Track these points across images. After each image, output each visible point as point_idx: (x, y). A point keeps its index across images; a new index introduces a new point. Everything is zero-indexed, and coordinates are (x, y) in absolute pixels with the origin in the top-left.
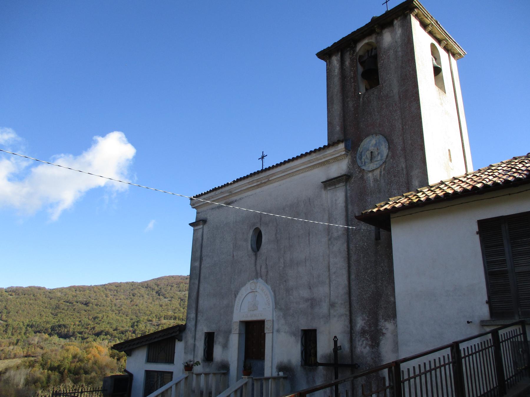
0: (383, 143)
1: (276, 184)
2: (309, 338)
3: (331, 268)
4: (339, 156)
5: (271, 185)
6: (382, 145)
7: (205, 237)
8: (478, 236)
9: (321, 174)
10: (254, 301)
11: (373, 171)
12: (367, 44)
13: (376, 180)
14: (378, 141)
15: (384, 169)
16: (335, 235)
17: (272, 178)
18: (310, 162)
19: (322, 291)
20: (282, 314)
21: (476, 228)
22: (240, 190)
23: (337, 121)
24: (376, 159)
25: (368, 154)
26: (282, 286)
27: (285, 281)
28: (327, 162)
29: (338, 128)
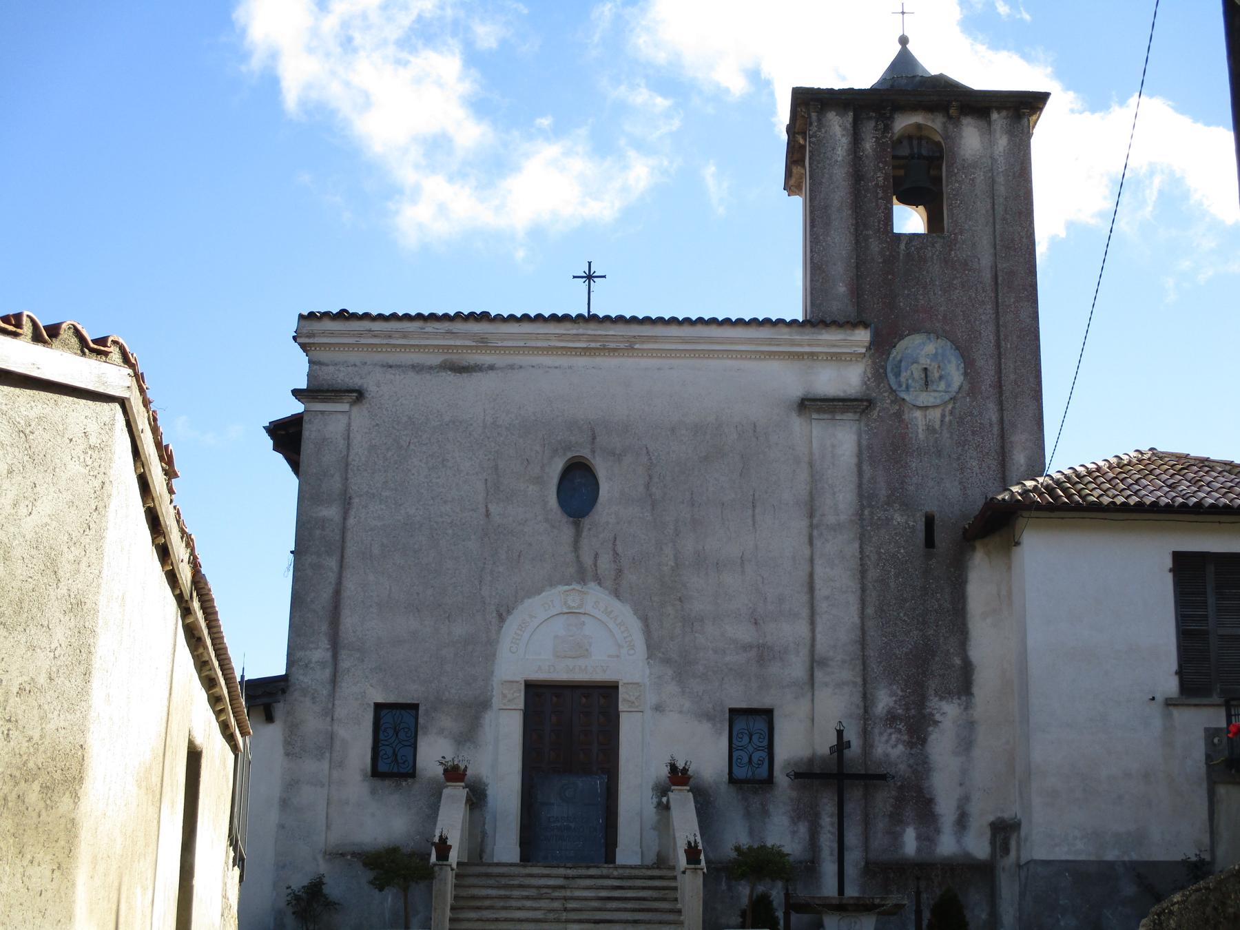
0: (953, 359)
2: (750, 725)
3: (817, 587)
6: (949, 362)
7: (357, 438)
8: (1170, 577)
9: (790, 380)
10: (566, 631)
11: (926, 411)
12: (919, 127)
13: (930, 429)
15: (951, 413)
16: (831, 519)
17: (645, 346)
18: (770, 341)
19: (792, 631)
20: (670, 672)
21: (1169, 563)
23: (840, 271)
24: (934, 387)
26: (670, 610)
27: (680, 600)
29: (842, 289)
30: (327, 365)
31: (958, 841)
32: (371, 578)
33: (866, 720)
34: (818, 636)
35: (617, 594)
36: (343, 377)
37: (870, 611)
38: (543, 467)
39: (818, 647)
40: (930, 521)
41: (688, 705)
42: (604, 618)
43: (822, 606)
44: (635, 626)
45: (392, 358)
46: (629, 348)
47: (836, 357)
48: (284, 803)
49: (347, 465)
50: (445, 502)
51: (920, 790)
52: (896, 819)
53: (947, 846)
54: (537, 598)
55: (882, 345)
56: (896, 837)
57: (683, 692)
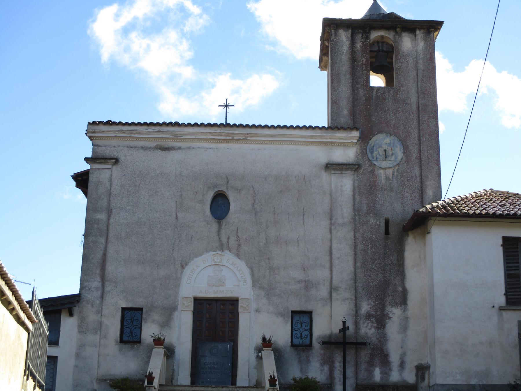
0: (398, 146)
1: (252, 146)
2: (302, 319)
6: (397, 147)
8: (501, 248)
9: (321, 155)
11: (385, 170)
12: (382, 37)
13: (387, 179)
14: (392, 142)
15: (397, 171)
18: (312, 137)
19: (321, 274)
21: (501, 242)
22: (194, 137)
24: (389, 159)
25: (382, 153)
29: (346, 112)
31: (400, 375)
33: (356, 317)
34: (334, 277)
35: (238, 256)
36: (108, 152)
37: (359, 264)
38: (203, 195)
39: (334, 281)
40: (387, 222)
41: (271, 309)
42: (232, 267)
43: (336, 262)
44: (247, 271)
46: (245, 139)
47: (343, 145)
48: (78, 355)
49: (110, 194)
51: (382, 350)
52: (371, 364)
53: (395, 377)
54: (200, 258)
55: (365, 139)
56: (370, 373)
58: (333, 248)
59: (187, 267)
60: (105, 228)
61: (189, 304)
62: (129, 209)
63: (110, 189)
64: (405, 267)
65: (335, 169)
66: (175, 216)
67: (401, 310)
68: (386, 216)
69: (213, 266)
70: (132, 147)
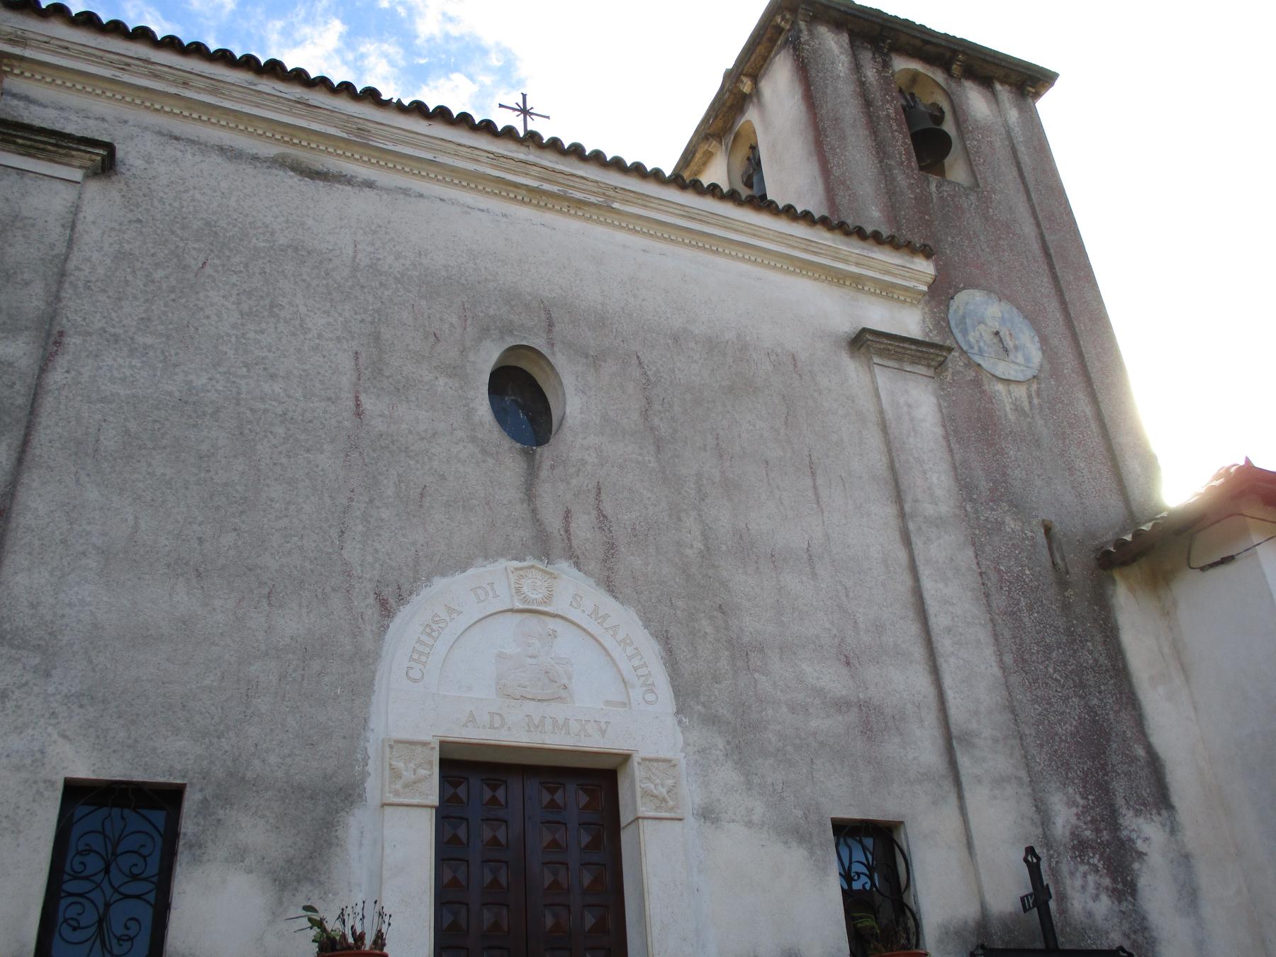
1: (621, 237)
4: (906, 289)
5: (599, 230)
22: (429, 156)
28: (857, 282)
30: (45, 107)
32: (92, 494)
34: (950, 694)
35: (610, 586)
37: (1008, 659)
38: (463, 351)
39: (953, 712)
41: (759, 809)
42: (593, 627)
43: (944, 644)
44: (650, 650)
45: (178, 127)
46: (599, 208)
47: (887, 291)
49: (63, 274)
50: (273, 377)
54: (459, 577)
55: (939, 294)
57: (749, 785)
58: (926, 595)
59: (404, 613)
60: (20, 401)
61: (422, 772)
62: (146, 347)
63: (66, 259)
64: (1134, 681)
65: (883, 353)
66: (352, 404)
67: (1163, 825)
68: (1043, 515)
69: (518, 617)
70: (177, 138)
